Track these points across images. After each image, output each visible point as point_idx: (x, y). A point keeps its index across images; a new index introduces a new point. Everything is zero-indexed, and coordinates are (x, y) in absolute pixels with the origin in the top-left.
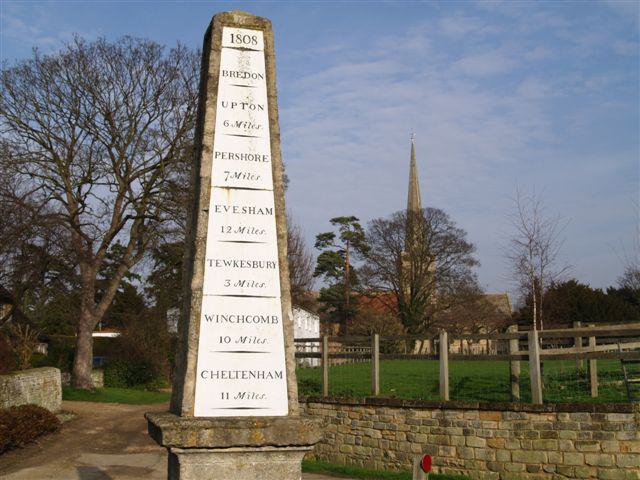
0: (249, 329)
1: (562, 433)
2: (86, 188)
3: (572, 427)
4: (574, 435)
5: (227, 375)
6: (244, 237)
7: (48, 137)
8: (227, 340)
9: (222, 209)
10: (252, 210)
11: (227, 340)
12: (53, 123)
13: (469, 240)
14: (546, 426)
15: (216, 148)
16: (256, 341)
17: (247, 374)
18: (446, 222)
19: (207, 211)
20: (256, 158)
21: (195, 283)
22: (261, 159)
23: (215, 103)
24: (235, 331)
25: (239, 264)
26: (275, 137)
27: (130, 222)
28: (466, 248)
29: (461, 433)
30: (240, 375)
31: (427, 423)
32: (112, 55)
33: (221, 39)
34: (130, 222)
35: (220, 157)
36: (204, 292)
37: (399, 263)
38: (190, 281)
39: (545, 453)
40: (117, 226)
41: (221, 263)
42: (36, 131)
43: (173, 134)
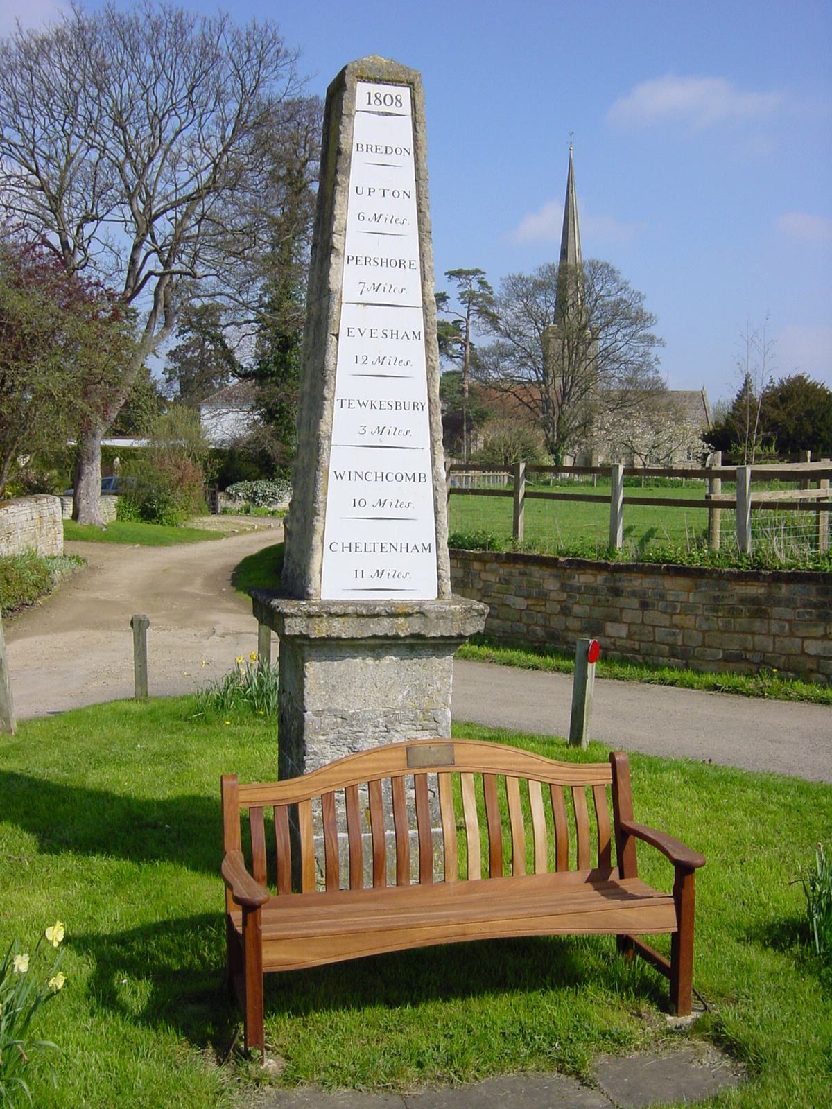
0: (391, 490)
1: (777, 611)
2: (88, 228)
3: (789, 602)
4: (788, 613)
5: (361, 548)
6: (384, 369)
7: (32, 154)
8: (362, 503)
9: (355, 332)
10: (394, 335)
11: (362, 503)
12: (39, 132)
13: (648, 307)
14: (754, 601)
15: (349, 251)
16: (399, 504)
17: (387, 547)
18: (615, 280)
19: (337, 336)
20: (401, 264)
21: (323, 427)
22: (407, 264)
23: (346, 190)
24: (372, 491)
25: (377, 405)
26: (424, 234)
27: (154, 280)
28: (640, 319)
29: (637, 606)
30: (378, 547)
31: (593, 590)
32: (123, 31)
33: (353, 100)
34: (154, 280)
35: (353, 262)
36: (333, 442)
37: (545, 342)
38: (317, 425)
39: (749, 637)
40: (135, 289)
41: (355, 404)
42: (15, 146)
43: (215, 145)
